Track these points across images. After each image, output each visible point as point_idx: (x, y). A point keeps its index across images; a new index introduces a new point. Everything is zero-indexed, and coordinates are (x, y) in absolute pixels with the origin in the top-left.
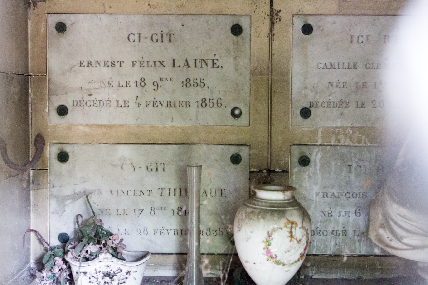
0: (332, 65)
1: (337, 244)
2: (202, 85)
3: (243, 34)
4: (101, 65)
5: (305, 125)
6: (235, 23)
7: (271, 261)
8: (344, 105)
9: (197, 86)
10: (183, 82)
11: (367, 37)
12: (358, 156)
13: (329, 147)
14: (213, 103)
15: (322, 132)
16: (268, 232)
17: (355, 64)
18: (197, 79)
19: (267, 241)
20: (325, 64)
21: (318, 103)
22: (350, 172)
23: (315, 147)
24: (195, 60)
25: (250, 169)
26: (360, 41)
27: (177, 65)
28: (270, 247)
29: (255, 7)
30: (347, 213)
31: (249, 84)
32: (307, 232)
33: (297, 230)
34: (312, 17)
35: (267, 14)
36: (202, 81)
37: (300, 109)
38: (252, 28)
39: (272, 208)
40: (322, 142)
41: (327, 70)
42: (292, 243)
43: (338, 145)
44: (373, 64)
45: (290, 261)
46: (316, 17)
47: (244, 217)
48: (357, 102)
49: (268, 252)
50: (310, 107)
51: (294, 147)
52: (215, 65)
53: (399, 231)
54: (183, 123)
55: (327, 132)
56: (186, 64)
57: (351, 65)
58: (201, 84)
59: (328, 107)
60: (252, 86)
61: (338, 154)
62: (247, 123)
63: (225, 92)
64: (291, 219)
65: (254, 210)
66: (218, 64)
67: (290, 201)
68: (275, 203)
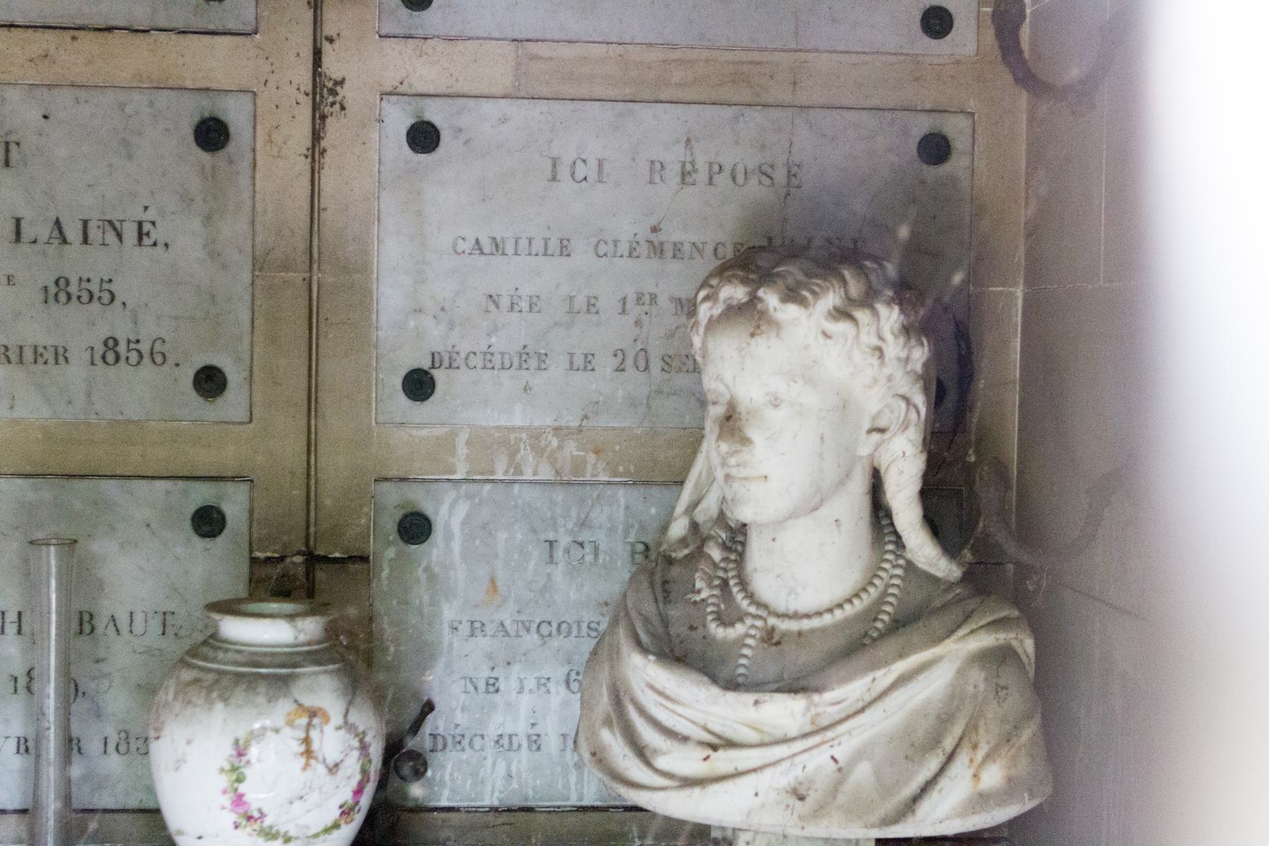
0: (497, 246)
1: (514, 774)
2: (106, 297)
3: (231, 148)
4: (125, 236)
5: (417, 421)
6: (206, 115)
7: (248, 830)
8: (533, 363)
9: (91, 300)
10: (46, 288)
11: (600, 164)
12: (574, 513)
13: (488, 487)
14: (139, 351)
15: (469, 443)
16: (237, 742)
17: (565, 243)
18: (89, 280)
19: (234, 769)
20: (477, 241)
21: (454, 355)
22: (551, 560)
23: (447, 485)
24: (85, 223)
25: (251, 551)
26: (580, 175)
27: (28, 232)
28: (242, 788)
29: (268, 68)
30: (543, 681)
31: (248, 297)
32: (361, 741)
33: (325, 736)
34: (439, 101)
35: (302, 89)
36: (106, 286)
37: (404, 372)
38: (258, 127)
39: (254, 670)
40: (468, 473)
41: (483, 257)
42: (309, 773)
43: (513, 482)
44: (616, 242)
45: (307, 827)
46: (450, 101)
47: (170, 697)
48: (571, 355)
49: (239, 800)
50: (433, 367)
51: (386, 485)
52: (145, 238)
53: (649, 735)
54: (45, 412)
55: (484, 442)
56: (56, 234)
57: (554, 245)
58: (102, 295)
59: (484, 368)
60: (258, 303)
61: (516, 506)
62: (242, 415)
63: (176, 318)
64: (308, 701)
65: (201, 675)
66: (153, 236)
67: (315, 647)
68: (266, 654)
